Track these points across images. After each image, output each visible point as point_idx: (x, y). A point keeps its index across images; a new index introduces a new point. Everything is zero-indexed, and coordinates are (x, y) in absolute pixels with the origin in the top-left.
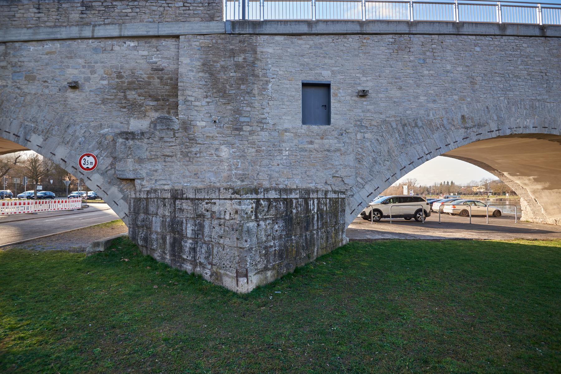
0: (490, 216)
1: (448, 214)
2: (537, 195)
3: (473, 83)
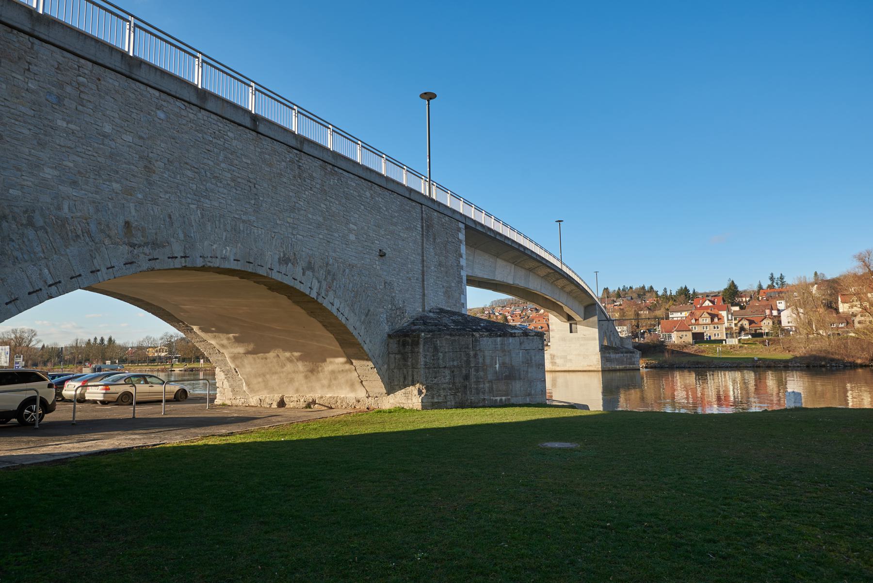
0: (168, 401)
1: (95, 402)
2: (238, 362)
3: (149, 169)
